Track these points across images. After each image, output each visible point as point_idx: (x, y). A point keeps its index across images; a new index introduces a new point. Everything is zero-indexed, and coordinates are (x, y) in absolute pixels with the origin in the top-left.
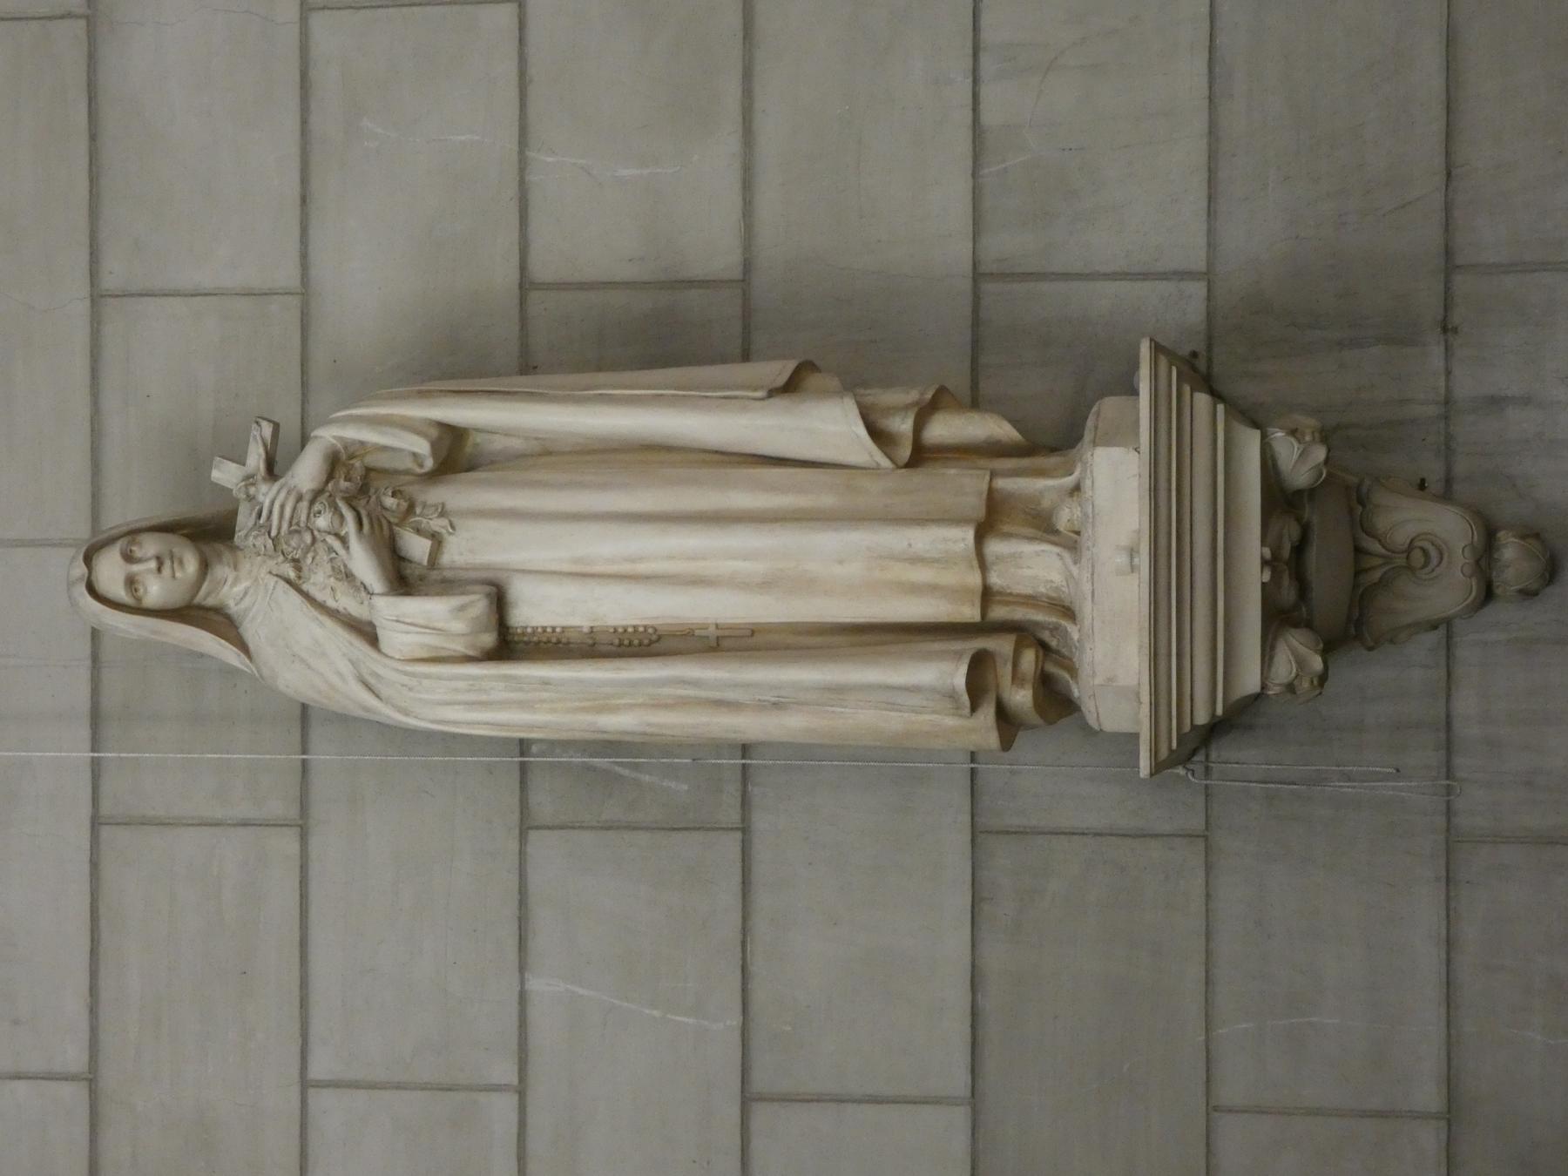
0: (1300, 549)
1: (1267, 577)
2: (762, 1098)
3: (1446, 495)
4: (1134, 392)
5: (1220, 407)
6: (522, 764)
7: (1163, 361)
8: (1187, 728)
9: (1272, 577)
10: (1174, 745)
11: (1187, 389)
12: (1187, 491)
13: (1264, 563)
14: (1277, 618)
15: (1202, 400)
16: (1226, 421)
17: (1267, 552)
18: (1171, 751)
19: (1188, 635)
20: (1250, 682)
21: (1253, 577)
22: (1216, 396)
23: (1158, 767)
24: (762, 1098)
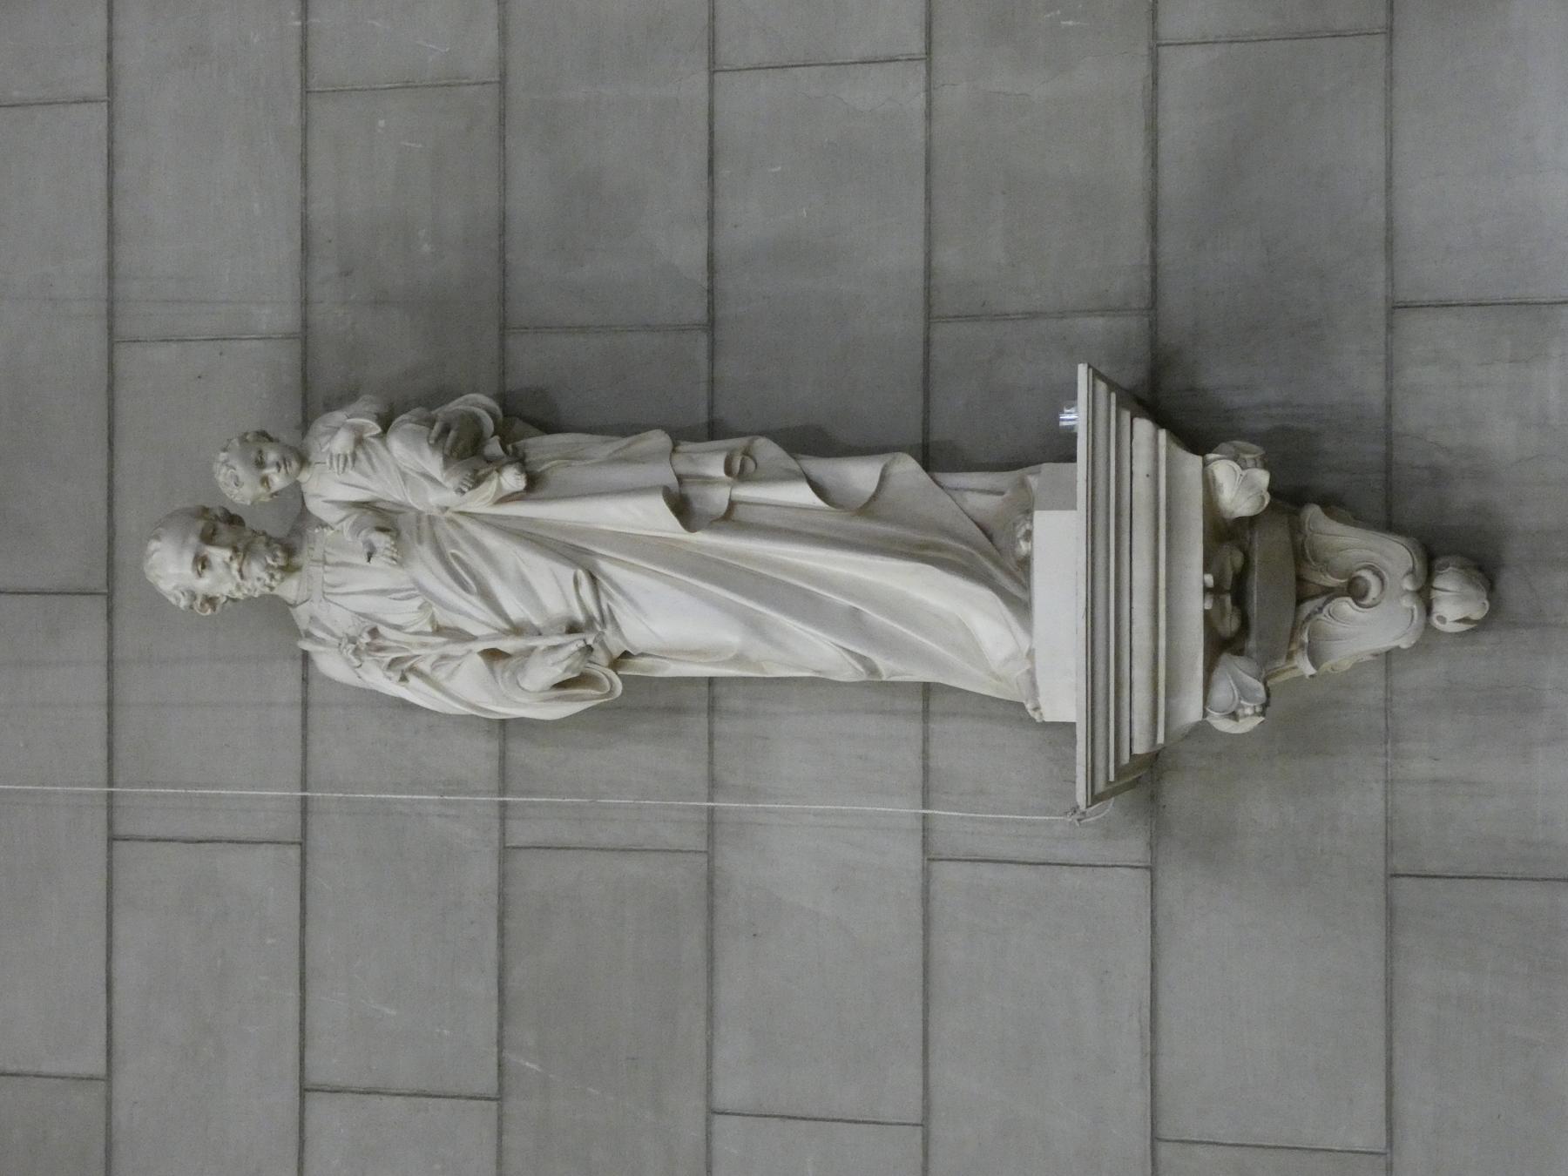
0: (1241, 578)
1: (1208, 606)
2: (318, 1090)
3: (1390, 526)
4: (1072, 458)
5: (1163, 434)
6: (304, 789)
7: (1102, 387)
8: (1126, 759)
9: (1215, 602)
10: (1112, 778)
11: (1126, 415)
12: (1126, 513)
13: (1206, 590)
14: (1220, 645)
15: (1144, 427)
16: (1168, 448)
17: (1209, 579)
18: (1108, 783)
19: (1126, 520)
20: (1191, 710)
21: (1195, 606)
22: (1160, 420)
23: (1095, 798)
24: (318, 1090)
